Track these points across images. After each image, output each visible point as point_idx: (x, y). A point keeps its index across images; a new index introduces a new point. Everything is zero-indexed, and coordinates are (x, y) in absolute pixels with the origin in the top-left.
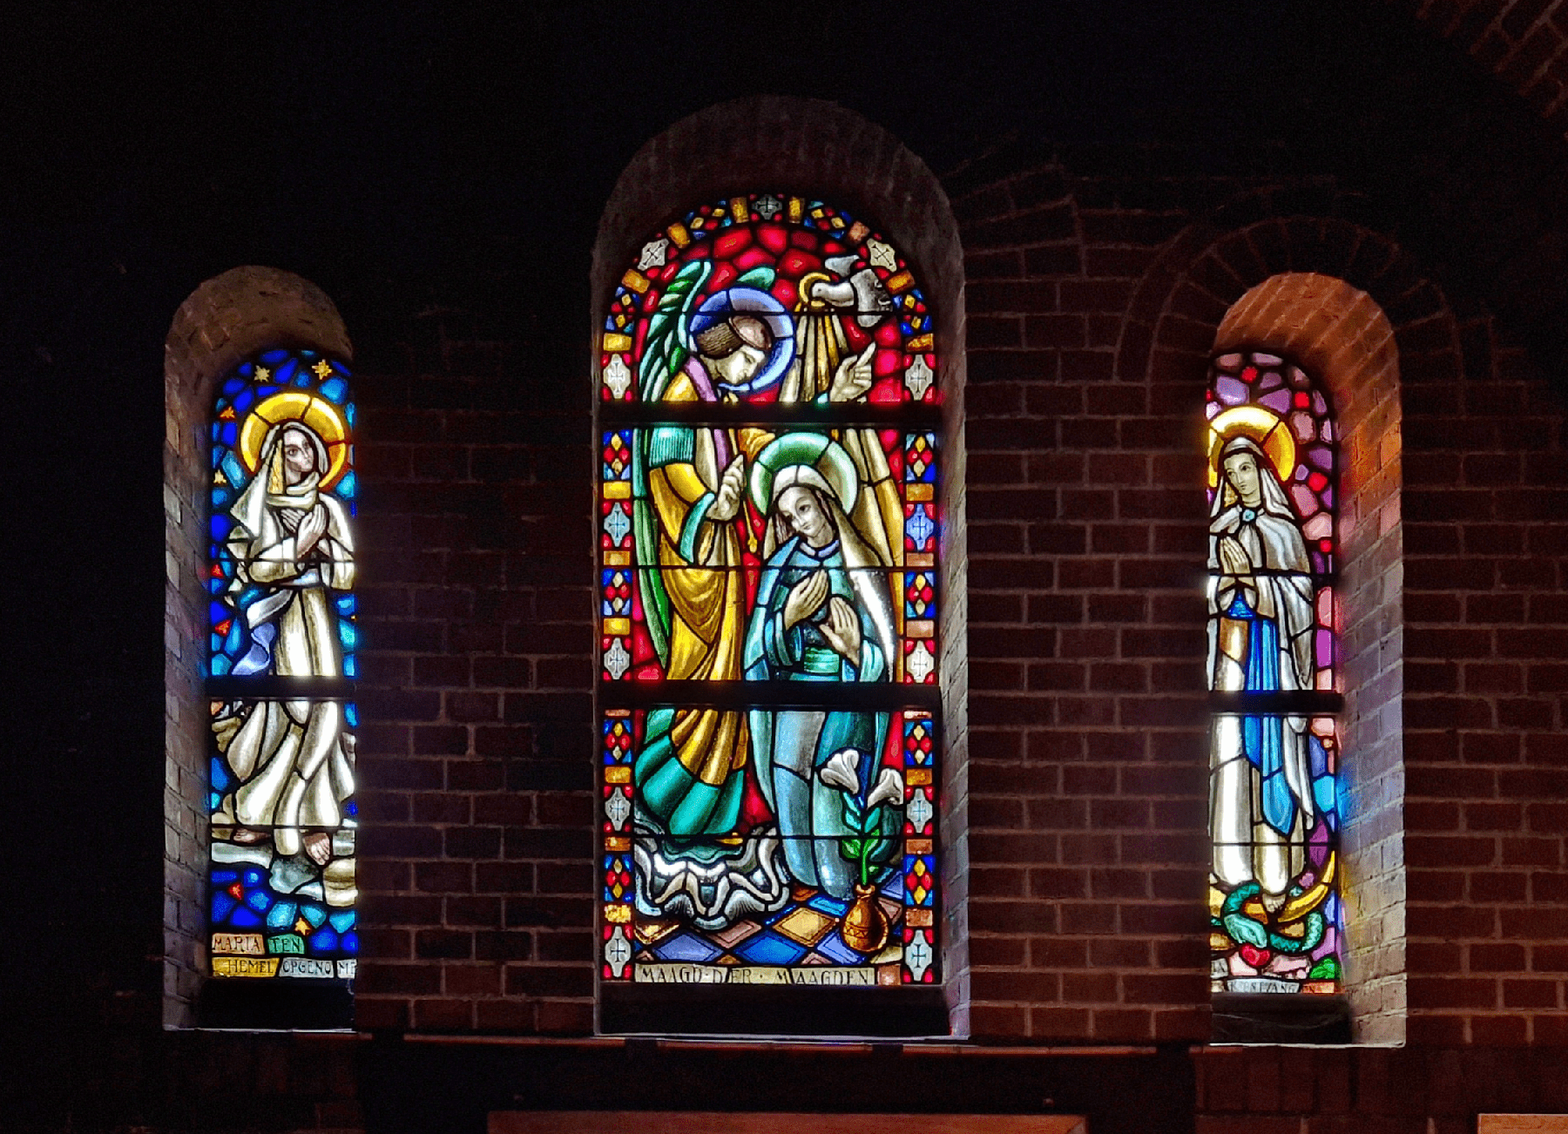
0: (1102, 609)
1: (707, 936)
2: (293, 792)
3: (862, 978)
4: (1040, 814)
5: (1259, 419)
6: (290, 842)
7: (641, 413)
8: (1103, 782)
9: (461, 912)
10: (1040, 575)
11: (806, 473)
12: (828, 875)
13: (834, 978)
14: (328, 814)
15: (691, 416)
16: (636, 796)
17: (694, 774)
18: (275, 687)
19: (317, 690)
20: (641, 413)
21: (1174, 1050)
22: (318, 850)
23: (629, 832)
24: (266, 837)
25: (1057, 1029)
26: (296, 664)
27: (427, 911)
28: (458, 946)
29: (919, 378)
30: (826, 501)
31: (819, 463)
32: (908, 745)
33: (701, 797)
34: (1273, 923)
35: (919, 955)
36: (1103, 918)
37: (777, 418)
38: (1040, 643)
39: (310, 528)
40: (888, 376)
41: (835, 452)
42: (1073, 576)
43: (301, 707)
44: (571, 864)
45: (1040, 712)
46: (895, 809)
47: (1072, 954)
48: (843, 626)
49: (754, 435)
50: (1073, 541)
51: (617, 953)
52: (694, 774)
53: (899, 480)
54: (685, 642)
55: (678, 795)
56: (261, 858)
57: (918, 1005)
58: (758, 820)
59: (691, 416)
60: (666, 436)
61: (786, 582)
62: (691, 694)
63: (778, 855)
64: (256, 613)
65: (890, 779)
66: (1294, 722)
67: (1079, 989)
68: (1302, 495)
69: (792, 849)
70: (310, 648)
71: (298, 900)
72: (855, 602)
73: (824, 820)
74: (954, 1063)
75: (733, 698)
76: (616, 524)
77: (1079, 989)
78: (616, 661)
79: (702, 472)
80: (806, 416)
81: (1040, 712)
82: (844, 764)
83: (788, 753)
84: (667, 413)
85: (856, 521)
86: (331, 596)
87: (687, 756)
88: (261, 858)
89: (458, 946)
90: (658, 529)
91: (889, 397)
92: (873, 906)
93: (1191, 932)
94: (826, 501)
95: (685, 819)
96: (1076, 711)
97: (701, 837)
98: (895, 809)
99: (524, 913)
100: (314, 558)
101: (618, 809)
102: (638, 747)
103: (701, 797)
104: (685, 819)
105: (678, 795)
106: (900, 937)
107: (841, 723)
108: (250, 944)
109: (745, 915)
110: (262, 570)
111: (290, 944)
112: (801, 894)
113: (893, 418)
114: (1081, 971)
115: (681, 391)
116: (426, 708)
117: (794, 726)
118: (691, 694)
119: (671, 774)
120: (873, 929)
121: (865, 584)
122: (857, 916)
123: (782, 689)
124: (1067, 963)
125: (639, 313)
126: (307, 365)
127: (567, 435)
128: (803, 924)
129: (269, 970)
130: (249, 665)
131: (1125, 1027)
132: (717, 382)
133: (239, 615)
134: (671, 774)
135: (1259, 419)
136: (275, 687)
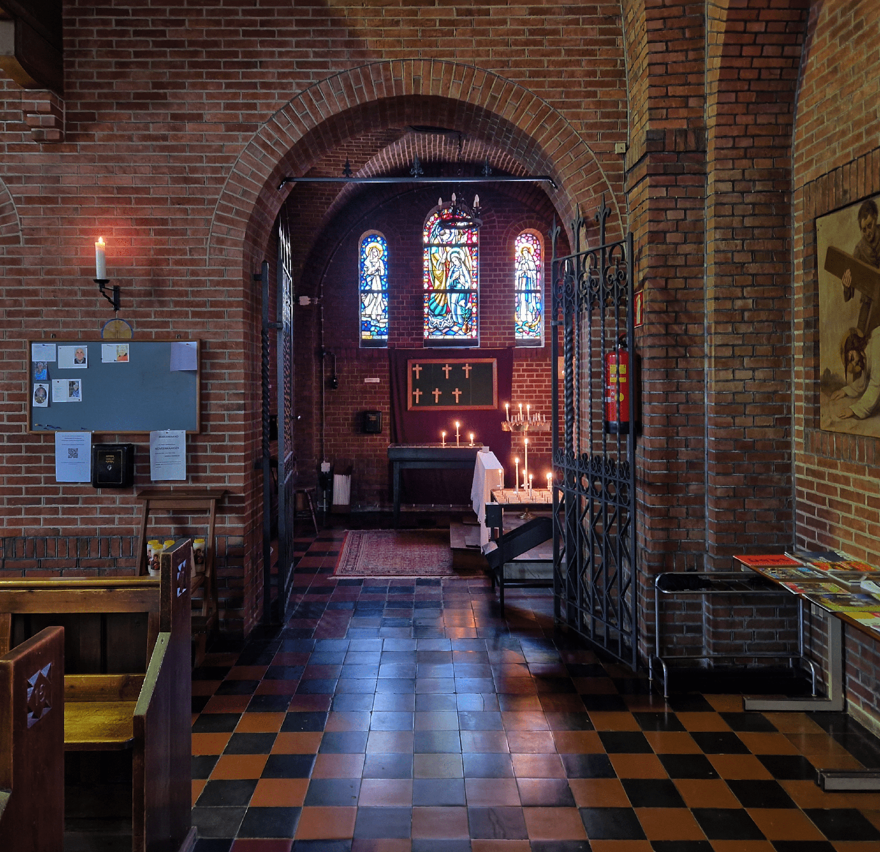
0: (500, 281)
1: (440, 331)
2: (374, 309)
3: (465, 337)
4: (490, 313)
5: (529, 245)
6: (374, 317)
7: (430, 245)
8: (500, 307)
9: (404, 329)
10: (490, 276)
11: (457, 255)
12: (460, 321)
13: (460, 337)
14: (380, 312)
15: (438, 245)
16: (429, 308)
17: (438, 304)
18: (371, 291)
19: (378, 292)
20: (430, 245)
21: (510, 348)
22: (378, 318)
23: (428, 314)
24: (370, 316)
25: (494, 345)
26: (374, 288)
27: (398, 329)
28: (403, 334)
29: (475, 239)
30: (460, 259)
31: (458, 253)
32: (473, 299)
33: (439, 308)
34: (530, 327)
35: (474, 333)
36: (499, 328)
37: (451, 246)
38: (491, 286)
39: (377, 265)
40: (469, 238)
41: (461, 251)
42: (495, 276)
43: (375, 295)
44: (419, 320)
45: (490, 297)
46: (470, 310)
47: (495, 334)
48: (462, 280)
49: (448, 248)
50: (495, 270)
51: (426, 334)
52: (438, 304)
53: (471, 255)
54: (437, 283)
55: (436, 308)
56: (369, 319)
57: (473, 342)
58: (448, 311)
59: (438, 245)
60: (434, 249)
61: (453, 272)
62: (437, 291)
63: (452, 317)
64: (369, 279)
65: (469, 305)
66: (533, 294)
67: (496, 339)
68: (535, 259)
69: (454, 317)
70: (377, 285)
71: (375, 326)
72: (464, 276)
73: (459, 312)
74: (477, 351)
75: (445, 292)
76: (426, 264)
77: (496, 339)
78: (426, 286)
79: (440, 255)
80: (457, 245)
81: (490, 297)
82: (462, 303)
83: (453, 301)
84: (433, 245)
85: (464, 263)
86: (380, 276)
87: (437, 301)
88: (369, 319)
89: (403, 334)
90: (433, 264)
91: (469, 242)
92: (467, 326)
93: (511, 326)
94: (460, 259)
95: (437, 312)
96: (496, 297)
97: (439, 315)
98: (470, 310)
99: (413, 329)
100: (378, 270)
101: (426, 310)
102: (429, 299)
103: (439, 308)
104: (437, 312)
105: (436, 308)
106: (471, 330)
107: (462, 295)
108: (368, 333)
109: (446, 327)
110: (369, 273)
111: (375, 333)
112: (455, 324)
113: (472, 246)
114: (862, 477)
115: (436, 242)
116: (399, 298)
117: (455, 296)
118: (437, 291)
119: (434, 305)
120: (467, 329)
121: (466, 273)
122: (464, 327)
123: (452, 290)
124: (830, 467)
125: (430, 229)
126: (376, 238)
127: (419, 249)
128: (455, 329)
129: (371, 338)
130: (367, 288)
131: (503, 345)
132: (442, 240)
133: (365, 280)
134: (434, 305)
135: (529, 245)
136: (371, 291)
